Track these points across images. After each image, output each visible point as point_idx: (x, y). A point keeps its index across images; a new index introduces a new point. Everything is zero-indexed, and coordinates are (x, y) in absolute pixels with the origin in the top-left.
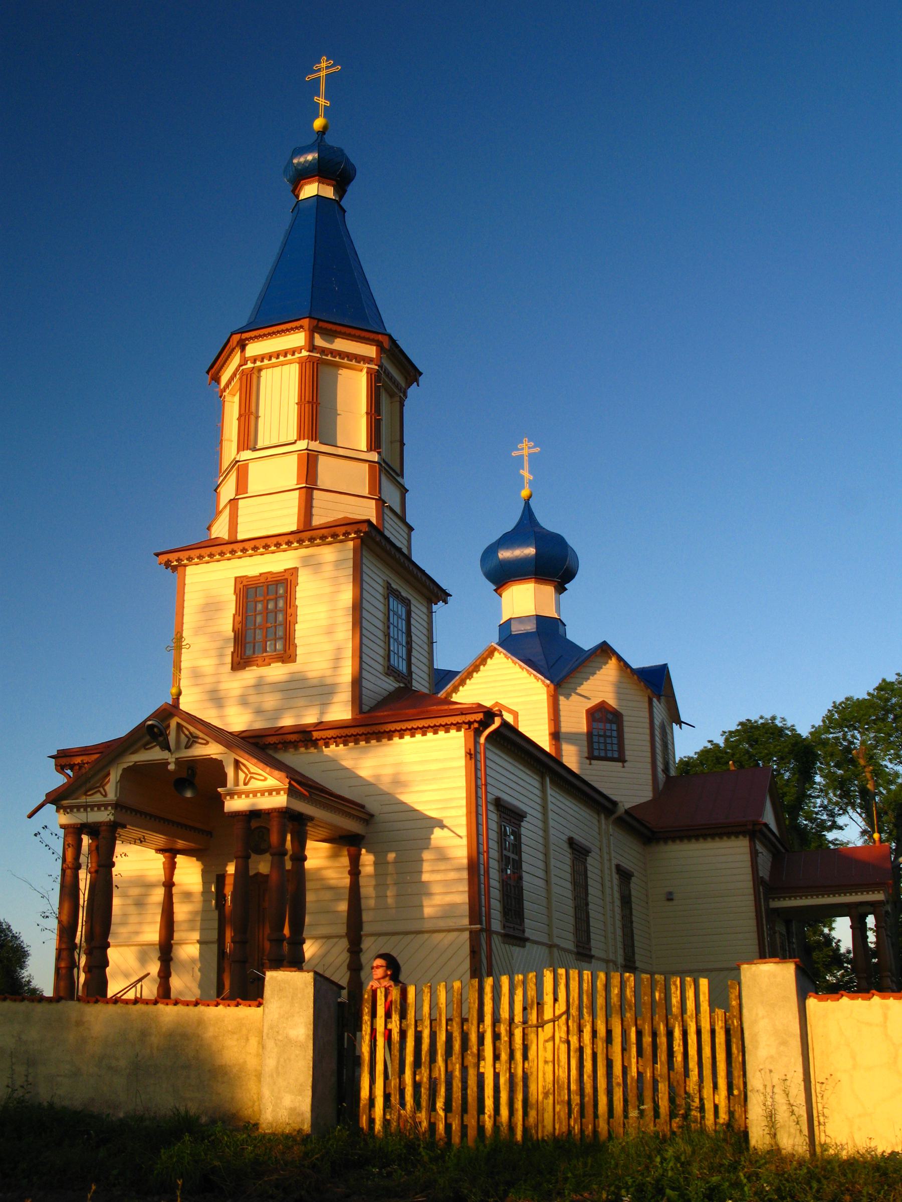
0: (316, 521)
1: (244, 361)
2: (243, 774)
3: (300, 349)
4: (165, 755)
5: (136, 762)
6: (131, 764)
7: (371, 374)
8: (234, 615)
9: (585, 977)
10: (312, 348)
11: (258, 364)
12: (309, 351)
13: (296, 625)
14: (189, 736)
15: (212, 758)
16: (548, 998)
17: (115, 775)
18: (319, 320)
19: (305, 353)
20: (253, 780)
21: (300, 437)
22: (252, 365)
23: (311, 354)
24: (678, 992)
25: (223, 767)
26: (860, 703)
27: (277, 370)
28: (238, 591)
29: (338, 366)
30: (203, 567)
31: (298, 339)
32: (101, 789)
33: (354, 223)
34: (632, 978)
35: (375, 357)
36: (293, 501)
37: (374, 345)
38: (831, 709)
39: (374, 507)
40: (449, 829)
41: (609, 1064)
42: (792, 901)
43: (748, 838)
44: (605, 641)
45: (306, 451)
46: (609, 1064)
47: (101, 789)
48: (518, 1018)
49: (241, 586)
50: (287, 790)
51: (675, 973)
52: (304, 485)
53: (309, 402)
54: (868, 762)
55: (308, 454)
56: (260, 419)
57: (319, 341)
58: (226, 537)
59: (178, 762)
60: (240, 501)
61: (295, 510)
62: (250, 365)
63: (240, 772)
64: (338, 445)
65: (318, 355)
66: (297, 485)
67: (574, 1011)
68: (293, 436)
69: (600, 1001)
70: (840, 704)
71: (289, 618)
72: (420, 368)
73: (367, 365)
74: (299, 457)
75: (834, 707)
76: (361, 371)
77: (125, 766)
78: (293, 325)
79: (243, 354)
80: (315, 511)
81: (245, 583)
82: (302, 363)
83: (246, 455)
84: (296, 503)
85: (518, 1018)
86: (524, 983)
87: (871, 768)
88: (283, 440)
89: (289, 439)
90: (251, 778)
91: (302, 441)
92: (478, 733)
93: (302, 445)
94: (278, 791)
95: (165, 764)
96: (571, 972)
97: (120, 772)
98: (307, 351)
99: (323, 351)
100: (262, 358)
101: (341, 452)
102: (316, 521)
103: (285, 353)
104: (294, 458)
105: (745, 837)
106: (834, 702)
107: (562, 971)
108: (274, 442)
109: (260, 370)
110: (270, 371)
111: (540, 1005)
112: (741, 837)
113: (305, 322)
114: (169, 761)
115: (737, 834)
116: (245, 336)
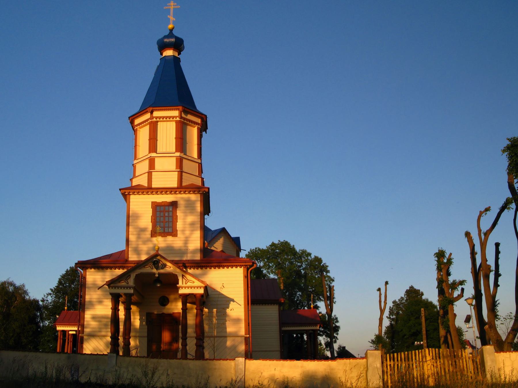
0: (184, 184)
1: (152, 118)
2: (185, 280)
3: (176, 117)
4: (155, 270)
5: (141, 272)
6: (139, 273)
7: (181, 123)
8: (152, 216)
9: (436, 350)
10: (181, 117)
11: (158, 119)
12: (180, 118)
13: (177, 223)
14: (163, 264)
15: (173, 273)
16: (427, 355)
17: (133, 276)
18: (185, 108)
19: (178, 119)
20: (189, 283)
21: (177, 151)
22: (156, 120)
23: (181, 120)
24: (460, 353)
25: (177, 277)
26: (263, 251)
27: (165, 123)
28: (153, 207)
29: (187, 125)
30: (137, 196)
31: (176, 113)
32: (126, 281)
33: (183, 65)
34: (449, 350)
35: (200, 123)
36: (175, 175)
37: (200, 119)
38: (249, 251)
39: (201, 180)
40: (236, 302)
41: (445, 369)
42: (285, 328)
43: (278, 305)
44: (224, 228)
45: (179, 157)
46: (445, 369)
47: (126, 281)
48: (421, 360)
49: (154, 205)
50: (204, 288)
51: (416, 350)
52: (179, 170)
53: (180, 138)
54: (282, 276)
55: (180, 158)
56: (158, 141)
57: (183, 115)
58: (146, 185)
59: (159, 274)
60: (153, 172)
61: (176, 179)
62: (154, 120)
63: (183, 279)
64: (187, 155)
65: (183, 120)
66: (176, 169)
67: (434, 358)
68: (174, 150)
69: (441, 355)
70: (253, 250)
71: (174, 220)
72: (208, 128)
73: (197, 126)
74: (177, 159)
75: (251, 251)
76: (194, 127)
77: (137, 273)
78: (175, 108)
79: (152, 115)
80: (183, 180)
81: (156, 204)
82: (177, 122)
83: (153, 155)
84: (177, 176)
85: (421, 360)
86: (422, 352)
87: (283, 278)
88: (168, 151)
89: (167, 151)
90: (188, 282)
91: (177, 153)
92: (248, 269)
93: (178, 154)
94: (200, 287)
95: (154, 274)
96: (433, 349)
97: (135, 275)
98: (179, 118)
99: (184, 119)
100: (160, 118)
101: (190, 158)
102: (184, 184)
103: (170, 117)
104: (174, 159)
105: (277, 305)
106: (251, 249)
107: (430, 349)
108: (164, 151)
109: (158, 122)
110: (162, 123)
111: (426, 357)
112: (275, 305)
113: (181, 108)
114: (156, 273)
115: (274, 304)
116: (154, 108)
